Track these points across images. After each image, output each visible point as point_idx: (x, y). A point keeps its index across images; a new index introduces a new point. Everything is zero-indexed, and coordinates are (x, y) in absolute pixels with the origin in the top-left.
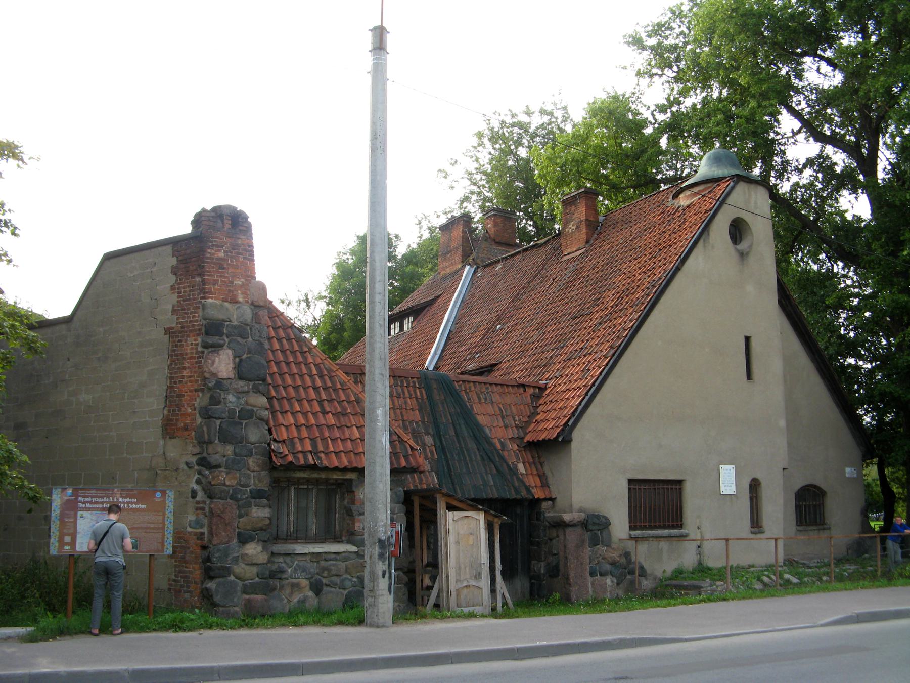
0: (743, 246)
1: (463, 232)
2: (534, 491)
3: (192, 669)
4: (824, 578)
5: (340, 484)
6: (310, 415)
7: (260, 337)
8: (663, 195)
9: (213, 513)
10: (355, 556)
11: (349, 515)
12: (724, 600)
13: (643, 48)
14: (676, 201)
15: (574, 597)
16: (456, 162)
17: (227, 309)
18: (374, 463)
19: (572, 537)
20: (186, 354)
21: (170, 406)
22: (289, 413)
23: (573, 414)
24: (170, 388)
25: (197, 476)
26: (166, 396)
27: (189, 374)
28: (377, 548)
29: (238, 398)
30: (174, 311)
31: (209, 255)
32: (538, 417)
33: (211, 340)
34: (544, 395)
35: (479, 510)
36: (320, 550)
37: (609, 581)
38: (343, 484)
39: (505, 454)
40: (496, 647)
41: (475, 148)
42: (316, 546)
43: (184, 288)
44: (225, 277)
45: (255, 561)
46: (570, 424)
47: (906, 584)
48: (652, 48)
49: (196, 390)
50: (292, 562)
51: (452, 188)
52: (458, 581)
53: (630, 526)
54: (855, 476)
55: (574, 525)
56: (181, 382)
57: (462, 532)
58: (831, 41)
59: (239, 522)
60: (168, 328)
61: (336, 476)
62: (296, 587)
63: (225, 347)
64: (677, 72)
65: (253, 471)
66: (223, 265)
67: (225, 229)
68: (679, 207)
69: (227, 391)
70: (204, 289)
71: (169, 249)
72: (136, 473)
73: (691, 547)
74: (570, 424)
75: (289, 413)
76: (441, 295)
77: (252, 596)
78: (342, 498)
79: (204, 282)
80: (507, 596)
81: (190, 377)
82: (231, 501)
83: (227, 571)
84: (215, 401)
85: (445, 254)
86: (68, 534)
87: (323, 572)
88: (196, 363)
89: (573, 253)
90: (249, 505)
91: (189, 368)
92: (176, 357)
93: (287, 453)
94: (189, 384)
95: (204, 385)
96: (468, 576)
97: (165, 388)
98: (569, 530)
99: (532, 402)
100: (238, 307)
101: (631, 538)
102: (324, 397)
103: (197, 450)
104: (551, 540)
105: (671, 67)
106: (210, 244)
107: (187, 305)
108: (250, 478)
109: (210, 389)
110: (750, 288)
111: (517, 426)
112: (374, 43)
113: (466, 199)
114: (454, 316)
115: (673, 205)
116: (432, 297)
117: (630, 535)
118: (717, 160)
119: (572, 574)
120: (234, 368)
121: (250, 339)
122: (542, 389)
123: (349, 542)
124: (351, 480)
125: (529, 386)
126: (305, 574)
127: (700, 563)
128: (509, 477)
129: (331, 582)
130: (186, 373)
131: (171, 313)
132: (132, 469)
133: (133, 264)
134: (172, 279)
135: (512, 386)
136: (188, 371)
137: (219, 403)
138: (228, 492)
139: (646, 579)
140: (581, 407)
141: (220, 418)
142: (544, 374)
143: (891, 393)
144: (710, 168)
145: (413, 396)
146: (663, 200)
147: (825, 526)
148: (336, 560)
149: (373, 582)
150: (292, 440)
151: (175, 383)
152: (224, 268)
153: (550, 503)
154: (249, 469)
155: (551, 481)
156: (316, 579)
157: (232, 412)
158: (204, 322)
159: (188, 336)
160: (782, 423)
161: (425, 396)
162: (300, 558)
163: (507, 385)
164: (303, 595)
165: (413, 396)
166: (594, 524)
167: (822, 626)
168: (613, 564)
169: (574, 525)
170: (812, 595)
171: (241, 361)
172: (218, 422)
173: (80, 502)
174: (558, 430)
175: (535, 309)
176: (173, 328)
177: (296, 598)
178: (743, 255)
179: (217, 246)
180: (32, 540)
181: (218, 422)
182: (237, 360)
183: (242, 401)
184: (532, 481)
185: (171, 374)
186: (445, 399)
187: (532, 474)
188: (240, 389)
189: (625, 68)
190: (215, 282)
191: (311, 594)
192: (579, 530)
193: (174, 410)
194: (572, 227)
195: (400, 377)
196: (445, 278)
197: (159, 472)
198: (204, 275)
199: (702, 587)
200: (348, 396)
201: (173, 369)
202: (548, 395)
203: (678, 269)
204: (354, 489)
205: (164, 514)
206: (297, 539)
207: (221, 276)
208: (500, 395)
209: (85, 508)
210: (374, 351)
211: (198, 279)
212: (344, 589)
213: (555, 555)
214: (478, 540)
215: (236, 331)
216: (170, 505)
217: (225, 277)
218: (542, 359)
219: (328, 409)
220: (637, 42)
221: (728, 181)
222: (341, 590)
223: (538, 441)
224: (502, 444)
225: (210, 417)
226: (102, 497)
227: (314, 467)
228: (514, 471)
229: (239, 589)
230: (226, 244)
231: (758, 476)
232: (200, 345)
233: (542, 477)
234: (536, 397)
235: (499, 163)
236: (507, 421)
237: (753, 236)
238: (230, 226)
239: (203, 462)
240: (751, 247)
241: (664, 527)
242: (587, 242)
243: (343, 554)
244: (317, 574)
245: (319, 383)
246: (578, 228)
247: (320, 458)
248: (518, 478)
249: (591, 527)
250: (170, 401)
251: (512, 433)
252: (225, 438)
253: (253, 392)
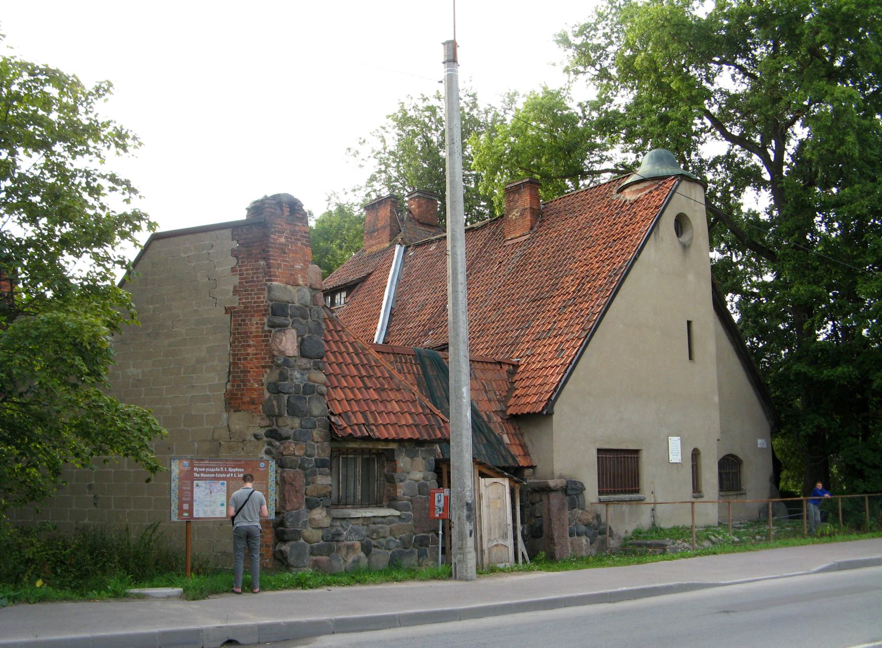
0: (685, 238)
1: (391, 211)
2: (519, 459)
3: (380, 617)
4: (758, 537)
5: (380, 454)
6: (355, 389)
7: (318, 318)
8: (605, 189)
9: (285, 481)
10: (396, 519)
11: (388, 482)
12: (715, 553)
13: (570, 45)
14: (621, 196)
15: (558, 556)
16: (364, 142)
17: (290, 291)
18: (461, 435)
19: (555, 500)
20: (251, 333)
21: (234, 381)
22: (338, 388)
23: (555, 390)
24: (234, 364)
25: (266, 447)
26: (229, 372)
27: (255, 352)
28: (465, 511)
29: (302, 375)
30: (236, 292)
31: (272, 241)
32: (517, 392)
33: (278, 320)
34: (518, 371)
35: (504, 476)
37: (584, 540)
38: (383, 453)
39: (492, 426)
40: (590, 593)
41: (384, 128)
42: (370, 510)
43: (246, 270)
44: (286, 261)
45: (321, 525)
46: (553, 398)
47: (880, 537)
48: (577, 47)
49: (263, 367)
50: (347, 525)
51: (361, 166)
52: (489, 540)
53: (599, 491)
54: (765, 446)
55: (556, 491)
56: (245, 359)
57: (491, 496)
58: (745, 52)
59: (306, 489)
60: (229, 308)
61: (381, 446)
62: (350, 548)
63: (290, 327)
64: (599, 71)
65: (318, 442)
66: (285, 250)
67: (285, 216)
68: (625, 201)
69: (291, 367)
70: (270, 272)
71: (228, 232)
72: (196, 444)
73: (646, 510)
74: (553, 398)
75: (338, 388)
76: (373, 272)
77: (319, 558)
78: (382, 467)
79: (269, 266)
80: (526, 553)
81: (256, 354)
82: (299, 470)
83: (298, 534)
84: (283, 377)
85: (371, 233)
86: (186, 502)
87: (372, 535)
88: (263, 341)
90: (314, 474)
91: (254, 346)
92: (239, 337)
93: (346, 425)
94: (255, 361)
95: (273, 362)
96: (497, 536)
97: (228, 364)
98: (552, 495)
99: (508, 379)
100: (299, 290)
101: (600, 502)
102: (364, 373)
103: (266, 422)
104: (533, 504)
105: (593, 65)
106: (273, 230)
107: (250, 286)
108: (314, 449)
109: (278, 366)
110: (691, 277)
111: (498, 400)
112: (448, 55)
113: (373, 179)
114: (393, 293)
115: (618, 198)
116: (363, 274)
117: (600, 499)
118: (658, 159)
119: (556, 535)
120: (298, 346)
121: (310, 320)
122: (516, 366)
123: (390, 506)
124: (393, 450)
125: (504, 363)
127: (654, 524)
128: (497, 446)
129: (379, 543)
130: (250, 350)
131: (232, 294)
132: (190, 440)
133: (187, 245)
134: (233, 261)
135: (491, 363)
136: (253, 348)
137: (286, 379)
138: (297, 461)
139: (613, 539)
140: (561, 384)
141: (288, 393)
142: (513, 352)
143: (805, 373)
144: (654, 166)
145: (412, 372)
146: (606, 193)
147: (742, 492)
148: (382, 523)
149: (462, 540)
150: (346, 413)
151: (239, 359)
152: (285, 253)
153: (531, 470)
154: (313, 441)
155: (531, 449)
156: (367, 541)
157: (297, 387)
158: (270, 303)
159: (252, 316)
160: (716, 399)
161: (421, 373)
162: (354, 522)
163: (486, 362)
165: (412, 372)
166: (573, 489)
167: (815, 572)
168: (587, 525)
169: (556, 491)
170: (778, 549)
171: (303, 340)
172: (286, 397)
173: (196, 472)
174: (543, 404)
175: (487, 290)
176: (235, 308)
177: (350, 559)
178: (685, 247)
179: (279, 232)
180: (74, 508)
181: (286, 397)
182: (300, 339)
183: (306, 377)
184: (516, 450)
185: (234, 351)
186: (438, 375)
187: (515, 444)
188: (304, 367)
189: (554, 65)
190: (279, 266)
191: (362, 554)
192: (560, 495)
193: (239, 386)
195: (398, 354)
196: (373, 256)
197: (222, 443)
198: (269, 259)
199: (666, 545)
200: (382, 373)
201: (236, 346)
202: (523, 372)
203: (636, 259)
204: (396, 458)
205: (267, 484)
206: (346, 504)
207: (284, 261)
208: (482, 372)
209: (200, 477)
210: (458, 335)
211: (262, 263)
212: (389, 549)
213: (539, 517)
214: (504, 503)
215: (298, 312)
217: (286, 261)
218: (507, 338)
219: (369, 385)
220: (564, 41)
221: (673, 179)
222: (387, 551)
223: (522, 414)
224: (488, 416)
225: (279, 392)
226: (215, 468)
227: (368, 439)
228: (500, 441)
229: (307, 550)
230: (286, 230)
231: (700, 447)
232: (266, 324)
233: (523, 446)
234: (512, 373)
235: (406, 146)
236: (490, 396)
238: (288, 214)
239: (274, 435)
240: (691, 239)
241: (625, 492)
242: (531, 229)
243: (388, 518)
244: (368, 536)
245: (357, 361)
246: (522, 215)
247: (372, 430)
248: (504, 447)
249: (569, 492)
250: (233, 377)
251: (496, 406)
252: (293, 411)
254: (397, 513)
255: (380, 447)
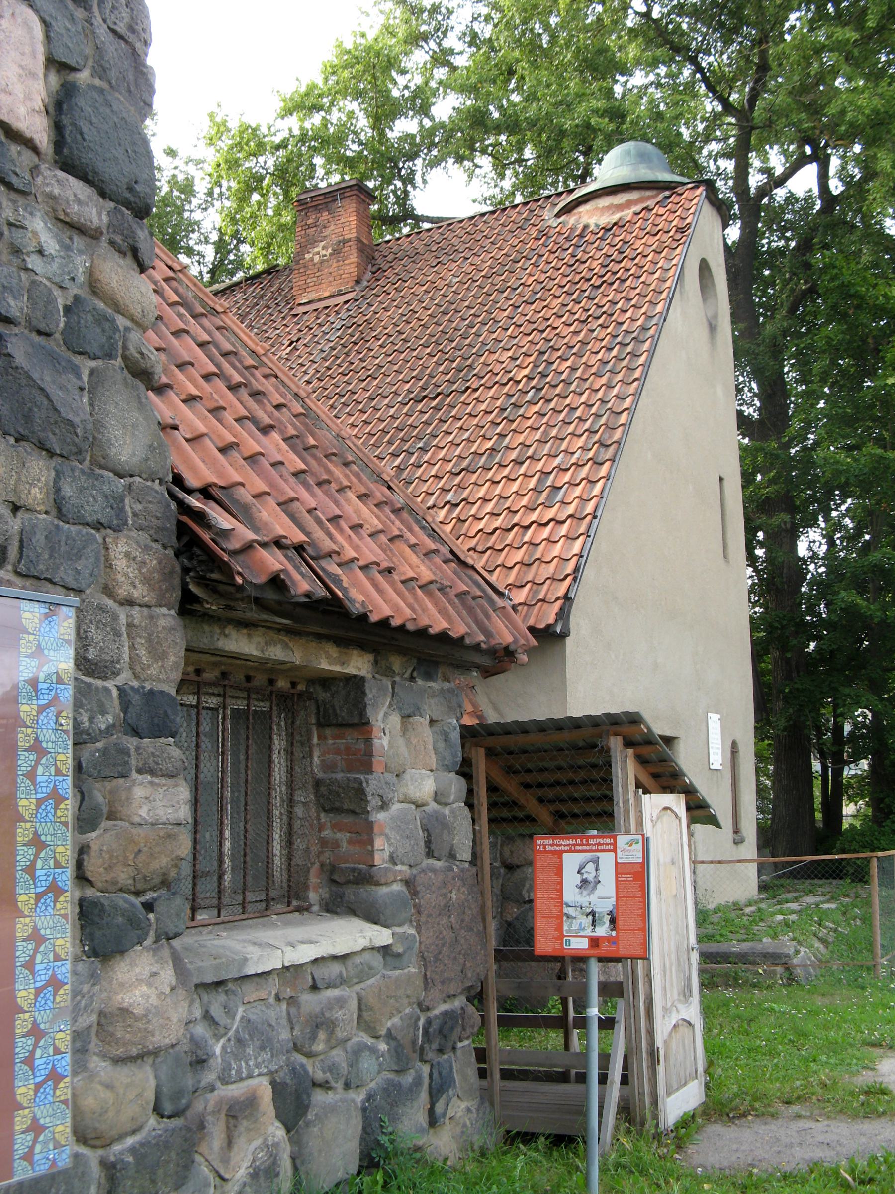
10: (377, 960)
14: (571, 220)
36: (304, 954)
65: (129, 603)
87: (313, 1038)
89: (320, 300)
124: (356, 683)
126: (266, 1056)
154: (108, 591)
164: (258, 1142)
194: (320, 251)
216: (47, 736)
237: (717, 299)
242: (358, 282)
243: (358, 960)
246: (336, 252)
253: (112, 243)
254: (382, 936)
255: (325, 665)
